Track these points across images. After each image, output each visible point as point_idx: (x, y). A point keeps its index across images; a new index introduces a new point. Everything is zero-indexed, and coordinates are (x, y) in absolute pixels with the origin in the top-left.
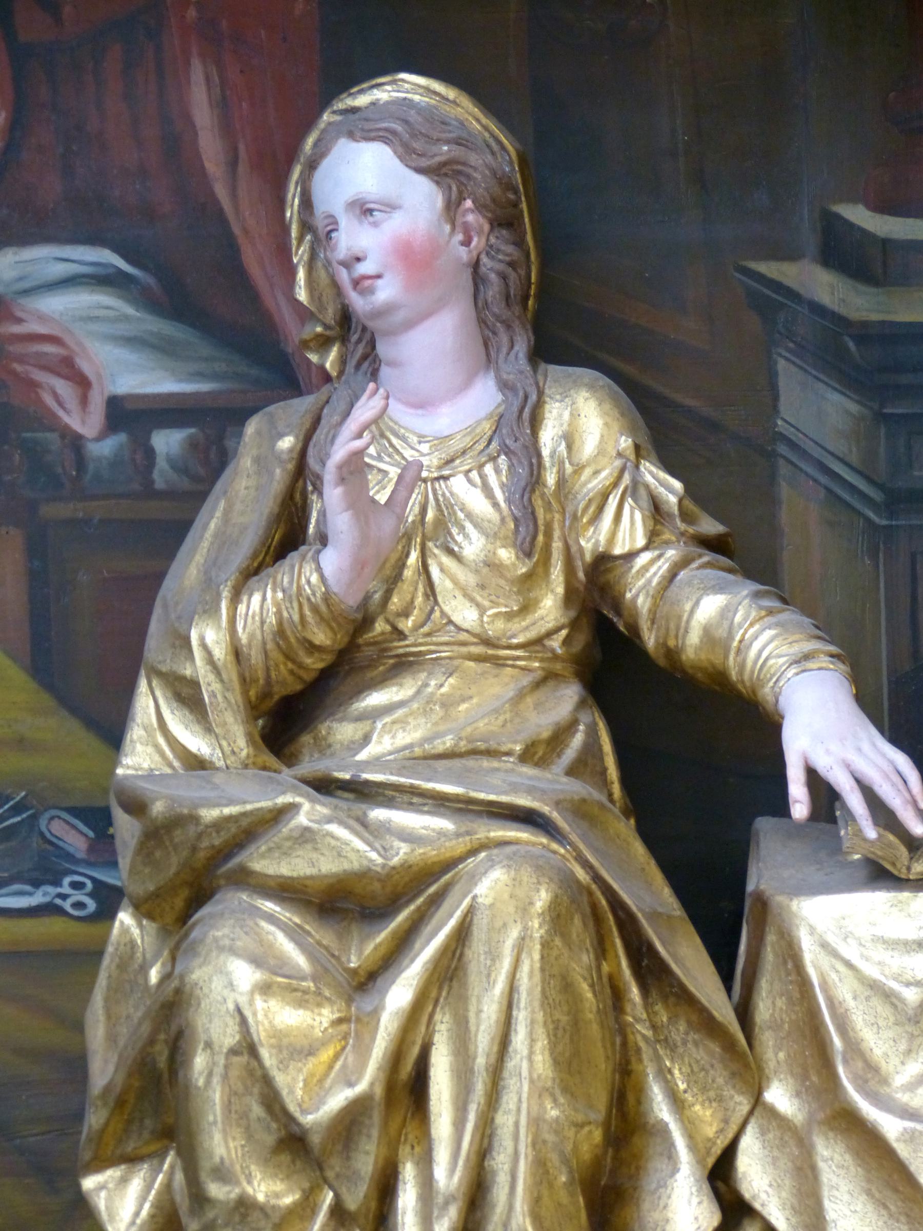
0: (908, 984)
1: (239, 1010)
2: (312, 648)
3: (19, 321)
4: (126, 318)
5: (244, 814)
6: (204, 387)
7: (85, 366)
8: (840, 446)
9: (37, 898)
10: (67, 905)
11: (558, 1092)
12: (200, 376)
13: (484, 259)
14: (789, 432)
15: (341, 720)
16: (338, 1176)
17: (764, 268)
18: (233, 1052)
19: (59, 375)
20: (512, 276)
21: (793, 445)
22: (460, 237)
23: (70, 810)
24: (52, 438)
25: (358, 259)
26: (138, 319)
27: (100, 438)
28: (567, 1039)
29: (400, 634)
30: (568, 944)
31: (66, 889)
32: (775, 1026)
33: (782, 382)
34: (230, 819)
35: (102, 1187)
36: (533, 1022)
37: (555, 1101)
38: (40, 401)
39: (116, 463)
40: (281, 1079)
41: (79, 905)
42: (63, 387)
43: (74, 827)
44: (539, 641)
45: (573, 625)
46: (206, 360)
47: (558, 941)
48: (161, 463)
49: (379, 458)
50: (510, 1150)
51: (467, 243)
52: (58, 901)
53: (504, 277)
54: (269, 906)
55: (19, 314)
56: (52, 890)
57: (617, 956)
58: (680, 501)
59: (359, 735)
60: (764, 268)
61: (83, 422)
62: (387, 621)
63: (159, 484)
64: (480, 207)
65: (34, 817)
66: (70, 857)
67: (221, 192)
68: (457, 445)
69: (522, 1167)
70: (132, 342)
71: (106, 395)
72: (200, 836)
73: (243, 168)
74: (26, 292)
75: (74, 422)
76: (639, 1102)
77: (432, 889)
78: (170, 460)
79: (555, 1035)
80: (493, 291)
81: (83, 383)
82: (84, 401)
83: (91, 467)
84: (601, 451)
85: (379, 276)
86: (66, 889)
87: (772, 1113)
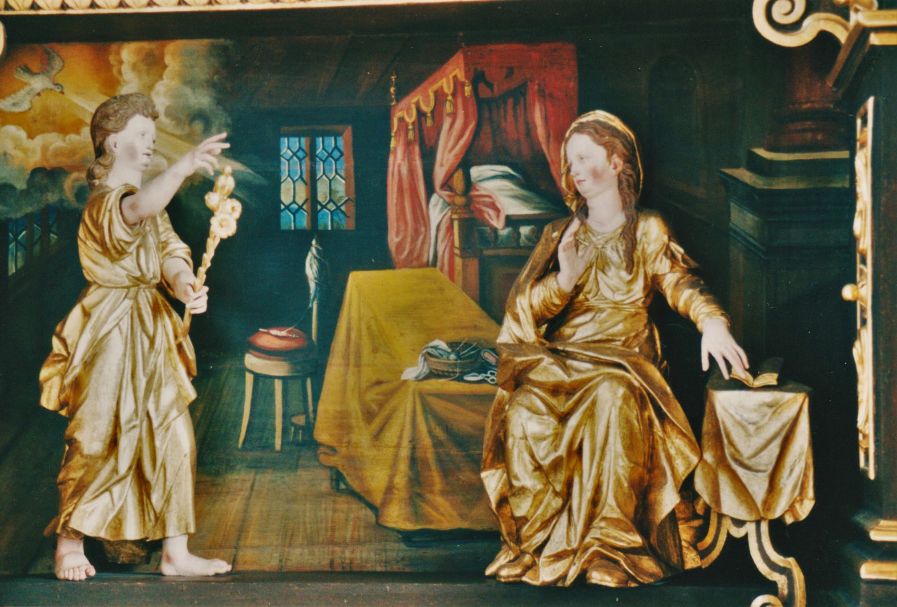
0: (750, 423)
1: (522, 425)
2: (555, 305)
3: (478, 190)
4: (512, 190)
5: (528, 360)
6: (537, 212)
7: (499, 206)
8: (751, 232)
9: (480, 377)
10: (489, 380)
11: (624, 456)
12: (535, 208)
13: (622, 174)
14: (734, 227)
15: (568, 327)
16: (553, 481)
17: (729, 171)
18: (521, 438)
19: (490, 208)
20: (631, 180)
21: (735, 232)
22: (612, 166)
23: (490, 349)
24: (488, 229)
25: (578, 175)
26: (516, 190)
27: (504, 228)
28: (628, 439)
29: (587, 300)
30: (629, 406)
31: (489, 375)
32: (708, 434)
33: (732, 210)
34: (523, 361)
35: (487, 477)
36: (616, 433)
37: (623, 459)
38: (483, 216)
39: (508, 237)
40: (534, 449)
41: (492, 380)
42: (492, 212)
43: (492, 355)
44: (633, 302)
45: (646, 296)
46: (538, 203)
47: (625, 407)
48: (523, 238)
49: (584, 240)
50: (607, 475)
51: (615, 168)
52: (486, 379)
53: (628, 180)
54: (536, 390)
55: (478, 188)
56: (484, 375)
57: (650, 410)
58: (683, 256)
59: (572, 333)
60: (729, 171)
61: (498, 224)
62: (584, 295)
63: (522, 245)
64: (619, 156)
65: (479, 352)
66: (491, 365)
67: (544, 147)
68: (608, 236)
69: (611, 481)
70: (515, 197)
71: (505, 214)
72: (515, 366)
73: (551, 139)
74: (480, 181)
75: (495, 223)
76: (657, 458)
77: (586, 387)
78: (525, 236)
79: (624, 438)
80: (625, 184)
81: (497, 210)
82: (498, 217)
83: (500, 238)
84: (656, 240)
85: (584, 180)
86: (489, 375)
87: (706, 462)
